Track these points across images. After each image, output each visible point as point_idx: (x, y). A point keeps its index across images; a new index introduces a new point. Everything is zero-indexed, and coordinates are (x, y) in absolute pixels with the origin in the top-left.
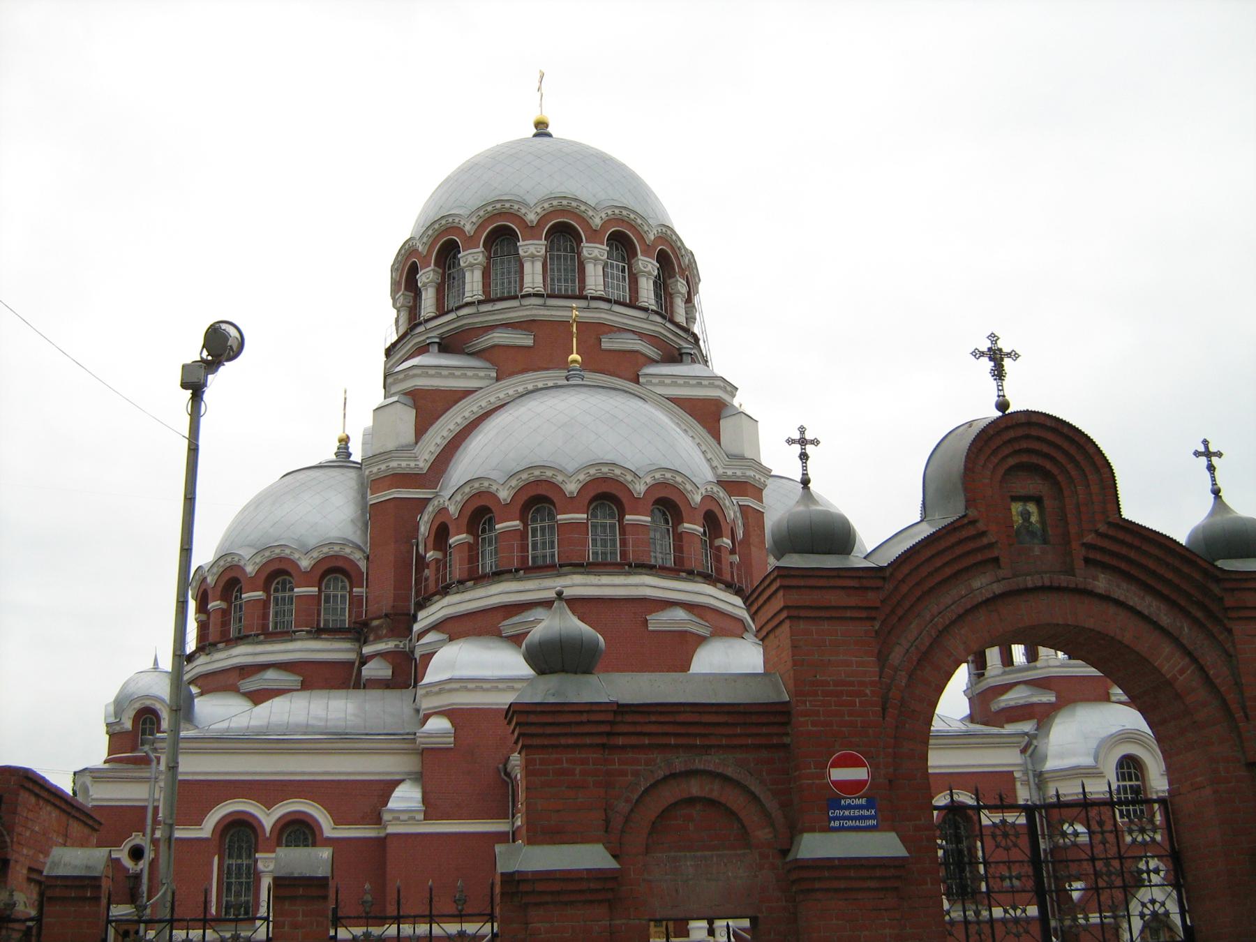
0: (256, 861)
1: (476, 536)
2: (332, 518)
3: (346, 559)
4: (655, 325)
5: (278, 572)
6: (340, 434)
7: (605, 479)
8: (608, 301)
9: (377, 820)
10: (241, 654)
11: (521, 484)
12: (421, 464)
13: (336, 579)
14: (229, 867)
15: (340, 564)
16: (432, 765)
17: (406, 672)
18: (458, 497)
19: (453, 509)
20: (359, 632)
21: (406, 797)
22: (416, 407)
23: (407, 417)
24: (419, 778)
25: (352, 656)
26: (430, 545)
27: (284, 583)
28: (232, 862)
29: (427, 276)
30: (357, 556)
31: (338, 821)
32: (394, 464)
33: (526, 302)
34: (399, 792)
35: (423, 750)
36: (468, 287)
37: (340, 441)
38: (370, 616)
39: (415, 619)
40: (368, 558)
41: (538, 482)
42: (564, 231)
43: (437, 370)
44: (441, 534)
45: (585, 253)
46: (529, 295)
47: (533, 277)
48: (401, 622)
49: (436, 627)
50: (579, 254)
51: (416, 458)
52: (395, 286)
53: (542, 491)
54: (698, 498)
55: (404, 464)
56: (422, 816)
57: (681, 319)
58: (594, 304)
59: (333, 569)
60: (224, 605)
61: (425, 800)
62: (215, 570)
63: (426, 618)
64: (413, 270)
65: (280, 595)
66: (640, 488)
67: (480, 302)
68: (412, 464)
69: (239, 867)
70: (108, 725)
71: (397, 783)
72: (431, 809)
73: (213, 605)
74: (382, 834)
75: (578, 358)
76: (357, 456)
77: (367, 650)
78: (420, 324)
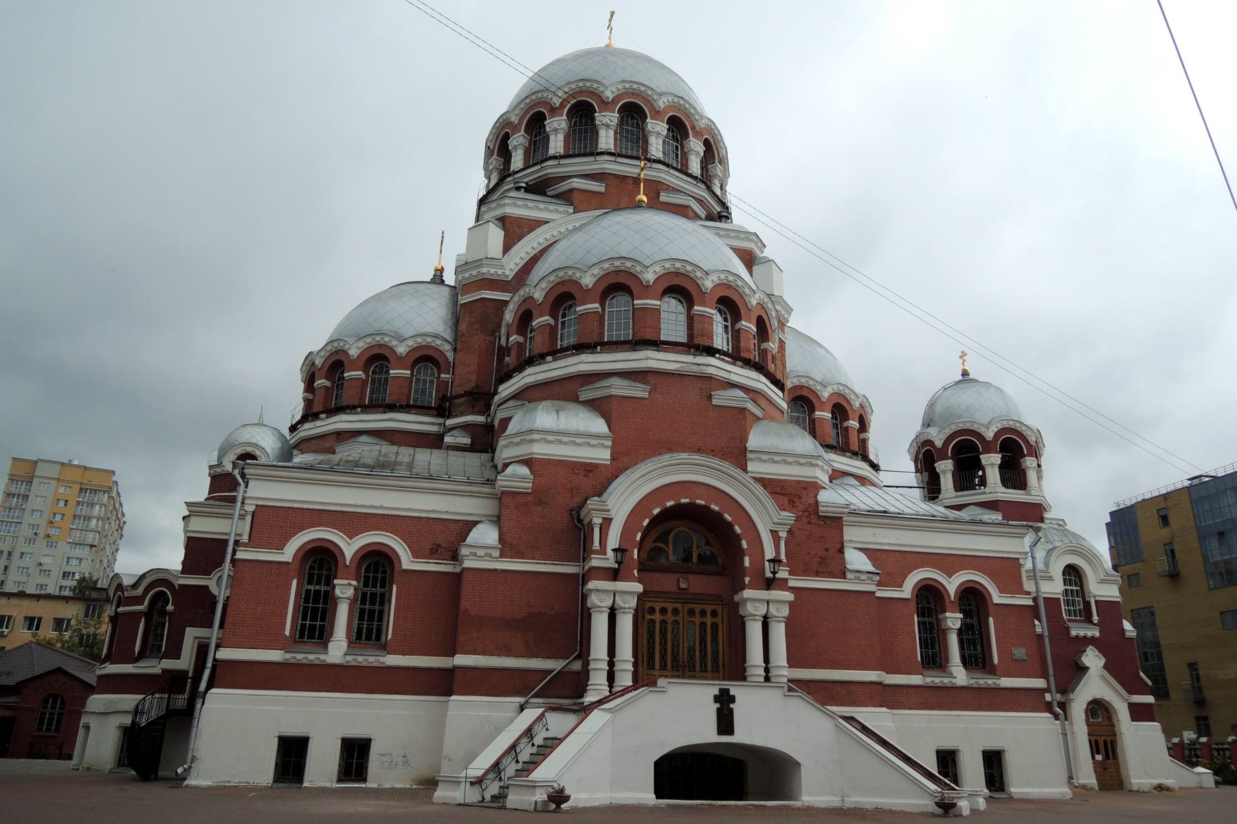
0: (334, 586)
1: (556, 320)
2: (428, 320)
3: (428, 347)
4: (701, 191)
5: (378, 358)
6: (437, 265)
7: (677, 274)
8: (668, 165)
9: (455, 557)
10: (343, 422)
11: (603, 273)
12: (507, 273)
13: (426, 368)
14: (308, 591)
15: (431, 353)
16: (507, 508)
17: (484, 440)
18: (543, 285)
19: (538, 295)
20: (442, 409)
21: (486, 535)
22: (504, 228)
23: (496, 235)
24: (497, 520)
25: (434, 429)
26: (514, 328)
27: (382, 366)
28: (312, 587)
29: (518, 141)
30: (446, 348)
31: (417, 554)
32: (484, 270)
33: (599, 158)
34: (475, 536)
35: (503, 492)
36: (552, 145)
37: (437, 270)
38: (454, 393)
39: (496, 393)
40: (455, 350)
41: (617, 272)
42: (633, 113)
43: (520, 207)
44: (525, 318)
45: (649, 127)
46: (602, 153)
47: (607, 139)
48: (481, 398)
49: (516, 396)
50: (643, 130)
51: (502, 267)
52: (489, 152)
53: (621, 279)
54: (754, 302)
55: (492, 271)
56: (497, 553)
57: (718, 192)
58: (654, 165)
59: (425, 358)
60: (328, 384)
61: (501, 540)
62: (322, 354)
63: (506, 389)
64: (507, 137)
65: (377, 376)
66: (708, 284)
67: (562, 157)
68: (500, 272)
69: (317, 592)
70: (211, 467)
71: (475, 523)
72: (507, 547)
73: (320, 382)
74: (458, 570)
75: (645, 199)
76: (450, 278)
77: (449, 422)
78: (510, 175)
